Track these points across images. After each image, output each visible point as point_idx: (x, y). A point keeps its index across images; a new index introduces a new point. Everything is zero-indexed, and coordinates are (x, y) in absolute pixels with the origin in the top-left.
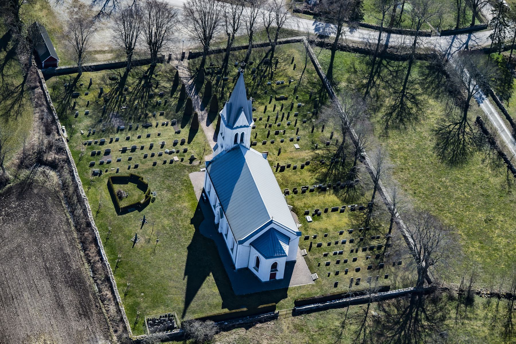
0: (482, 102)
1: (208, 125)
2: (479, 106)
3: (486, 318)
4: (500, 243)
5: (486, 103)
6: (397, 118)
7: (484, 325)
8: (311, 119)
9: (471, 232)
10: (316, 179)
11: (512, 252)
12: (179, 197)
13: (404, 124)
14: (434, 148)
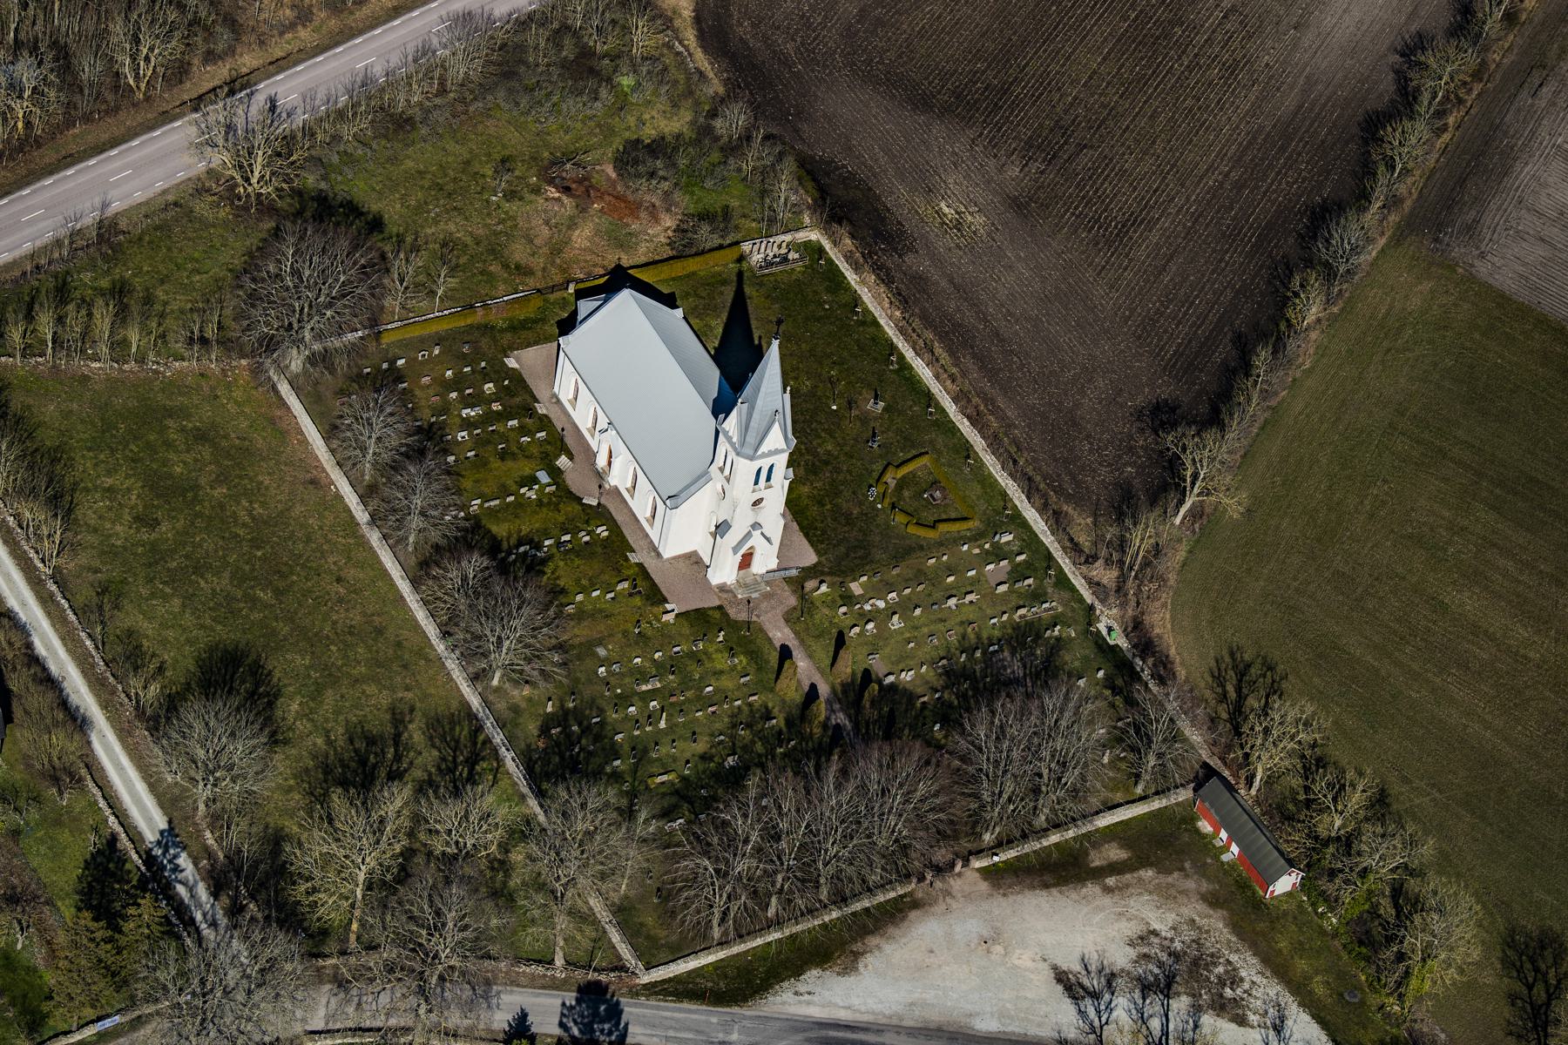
0: (162, 832)
1: (813, 687)
2: (170, 822)
4: (127, 477)
5: (152, 830)
6: (375, 766)
7: (166, 303)
8: (583, 732)
9: (190, 495)
11: (102, 456)
12: (821, 504)
13: (356, 751)
14: (277, 695)
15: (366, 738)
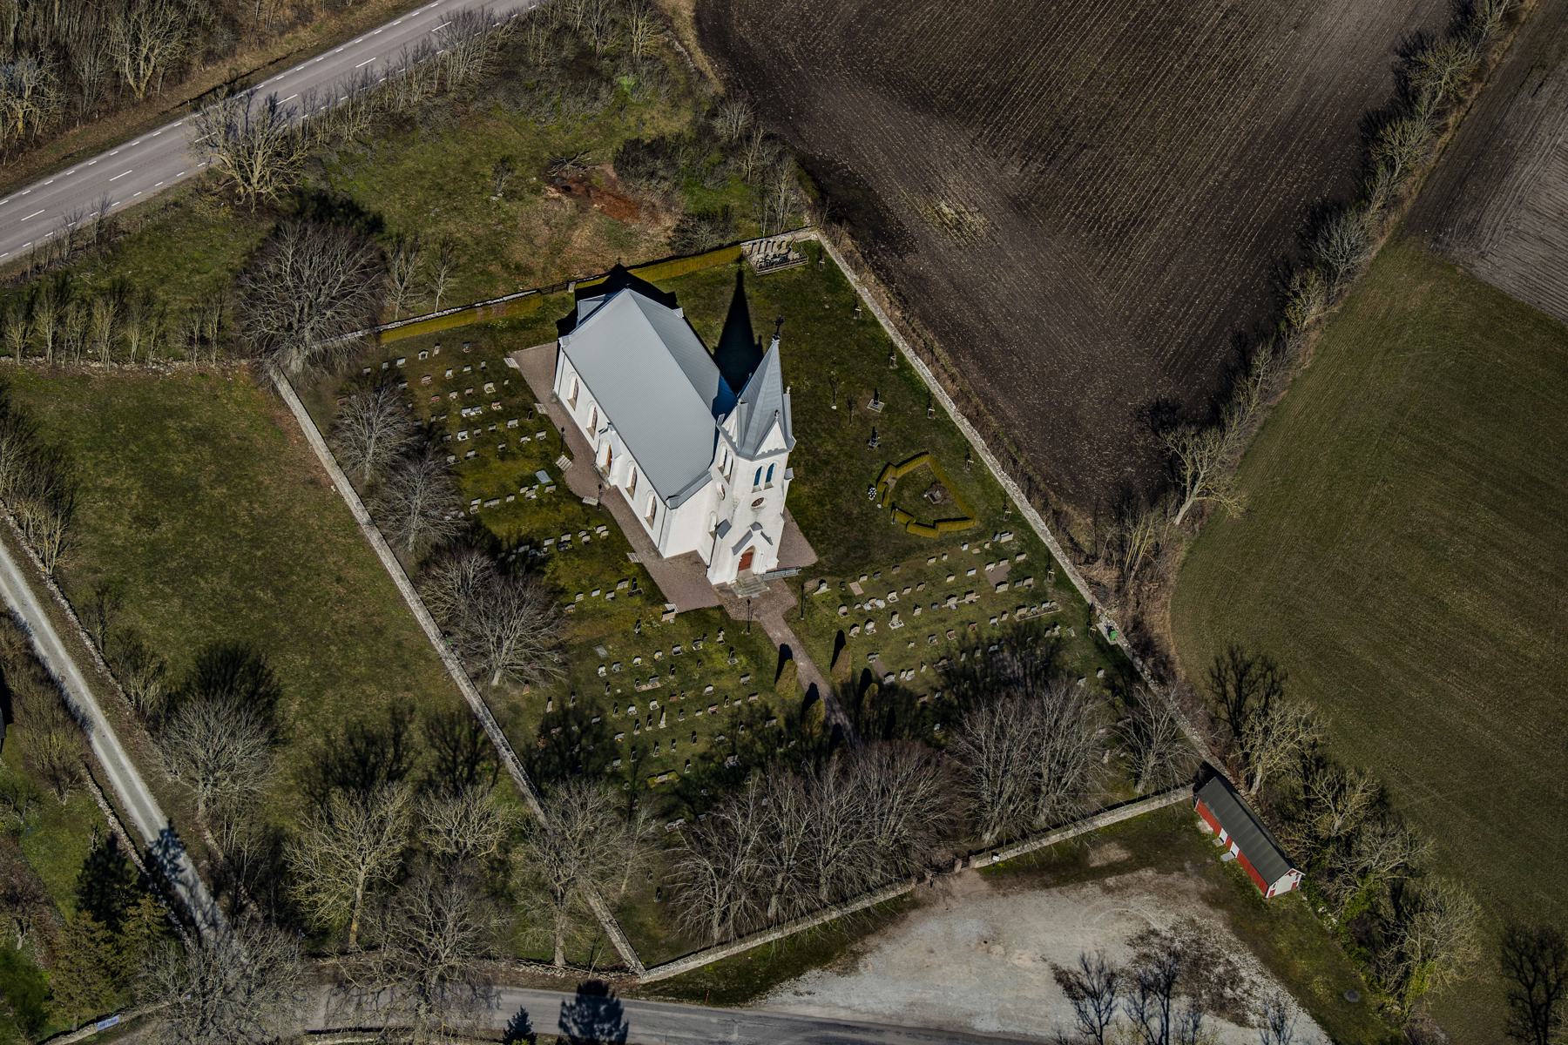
0: (162, 833)
2: (170, 822)
3: (162, 315)
6: (375, 766)
7: (165, 304)
8: (583, 732)
10: (544, 573)
11: (102, 457)
12: (821, 504)
14: (277, 696)
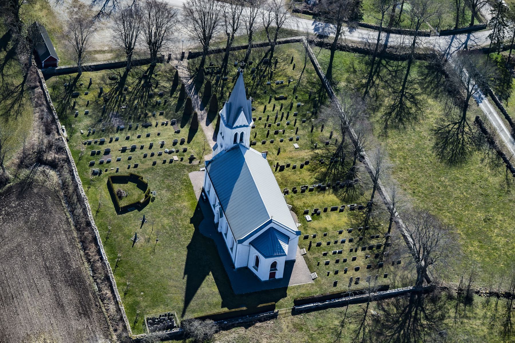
0: (481, 102)
1: (207, 125)
2: (478, 105)
3: (485, 317)
4: (499, 242)
5: (485, 102)
6: (396, 118)
7: (483, 324)
8: (310, 118)
9: (470, 232)
10: (316, 178)
11: (511, 252)
12: (179, 196)
13: (403, 124)
14: (433, 148)
15: (398, 129)
